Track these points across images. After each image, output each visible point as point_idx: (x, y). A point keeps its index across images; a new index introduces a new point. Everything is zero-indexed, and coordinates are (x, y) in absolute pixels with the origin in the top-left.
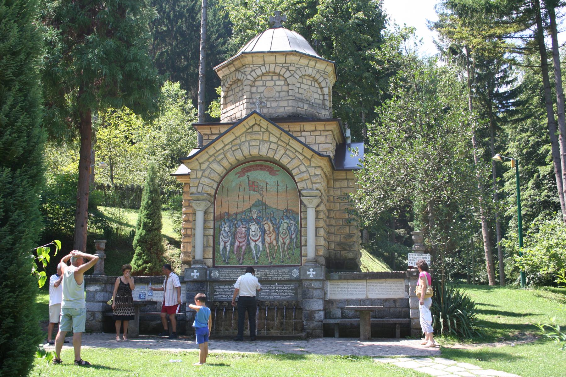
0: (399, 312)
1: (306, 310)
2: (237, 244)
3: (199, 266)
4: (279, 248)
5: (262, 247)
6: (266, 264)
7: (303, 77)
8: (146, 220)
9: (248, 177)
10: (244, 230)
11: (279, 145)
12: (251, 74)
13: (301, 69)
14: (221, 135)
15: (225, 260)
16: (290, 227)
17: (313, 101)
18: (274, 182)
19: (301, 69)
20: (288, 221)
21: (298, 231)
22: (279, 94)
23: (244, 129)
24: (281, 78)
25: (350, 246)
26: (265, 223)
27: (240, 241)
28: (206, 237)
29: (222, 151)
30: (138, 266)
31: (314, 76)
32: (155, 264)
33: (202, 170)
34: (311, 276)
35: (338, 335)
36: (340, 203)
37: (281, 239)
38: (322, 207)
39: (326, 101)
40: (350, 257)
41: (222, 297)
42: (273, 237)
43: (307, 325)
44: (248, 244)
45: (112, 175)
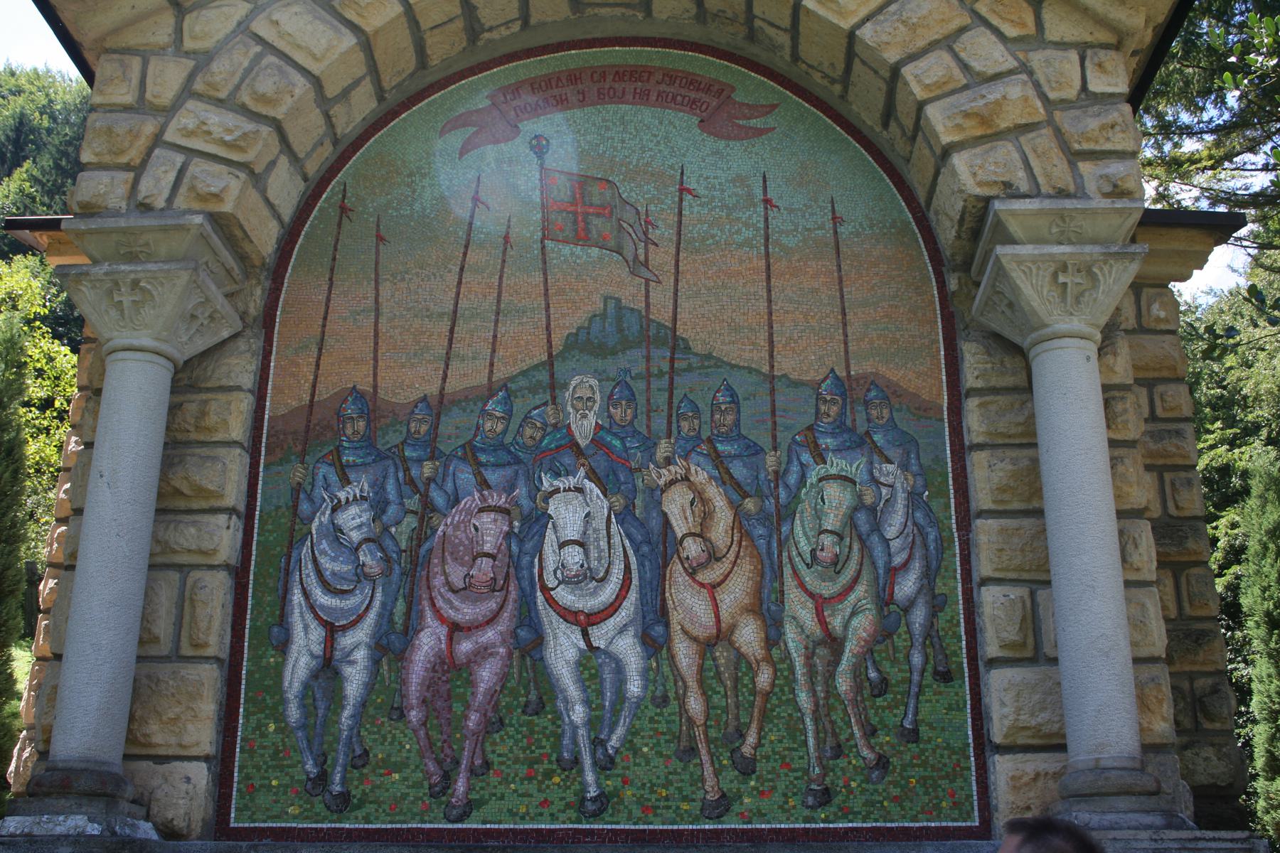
2: (429, 641)
4: (791, 680)
10: (491, 530)
15: (322, 779)
16: (872, 510)
18: (740, 180)
20: (855, 466)
21: (943, 544)
33: (187, 54)
37: (799, 609)
42: (735, 593)
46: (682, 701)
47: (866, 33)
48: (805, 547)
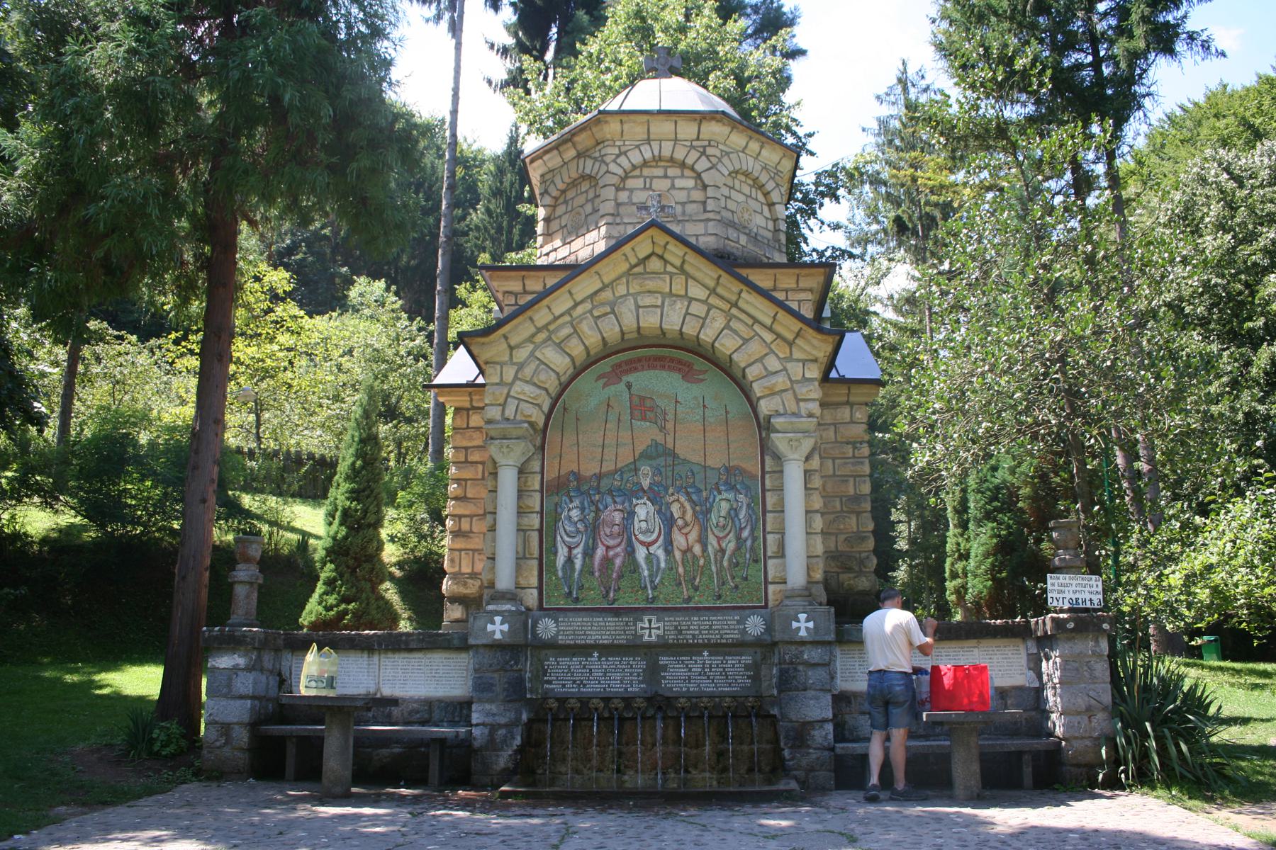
1: (791, 721)
2: (600, 552)
3: (508, 607)
4: (710, 562)
5: (666, 561)
7: (735, 173)
8: (348, 503)
9: (629, 386)
10: (618, 517)
13: (731, 155)
14: (548, 292)
15: (570, 593)
16: (736, 510)
18: (695, 398)
19: (731, 155)
20: (730, 496)
21: (757, 520)
23: (625, 267)
24: (687, 173)
26: (672, 499)
27: (609, 546)
28: (522, 533)
29: (567, 318)
30: (328, 609)
31: (757, 175)
32: (368, 604)
33: (515, 364)
34: (803, 633)
36: (834, 459)
37: (712, 540)
40: (861, 588)
41: (564, 686)
42: (693, 536)
43: (792, 759)
44: (631, 552)
45: (258, 433)
46: (677, 569)
47: (735, 356)
48: (715, 522)
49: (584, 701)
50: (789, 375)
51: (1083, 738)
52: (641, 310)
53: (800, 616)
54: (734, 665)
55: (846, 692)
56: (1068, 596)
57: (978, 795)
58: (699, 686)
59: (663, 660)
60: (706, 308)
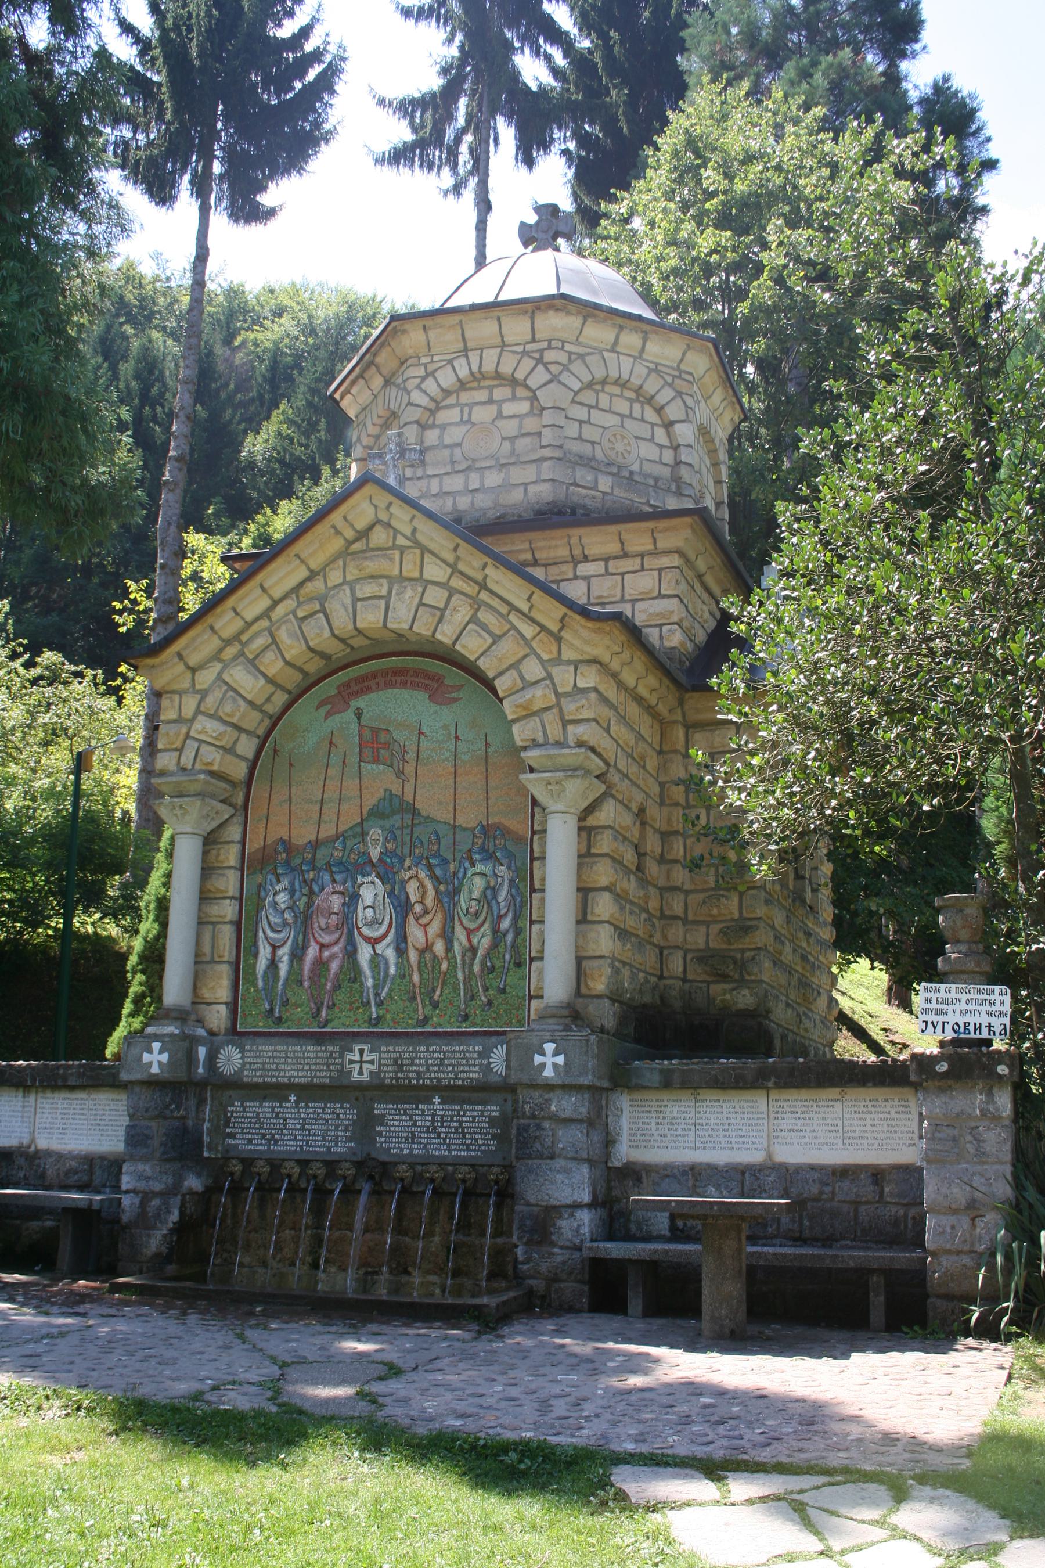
0: (896, 1222)
1: (528, 1204)
2: (312, 952)
3: (172, 1029)
4: (455, 967)
5: (397, 964)
6: (408, 1026)
9: (359, 714)
10: (336, 902)
11: (452, 592)
12: (423, 386)
13: (588, 359)
15: (271, 1011)
16: (494, 888)
17: (635, 467)
18: (445, 727)
19: (588, 359)
21: (523, 903)
22: (513, 443)
23: (338, 544)
24: (521, 392)
25: (742, 966)
26: (408, 874)
29: (265, 623)
31: (638, 382)
33: (197, 692)
34: (548, 1072)
35: (640, 1308)
37: (460, 935)
38: (607, 814)
39: (683, 466)
40: (741, 1006)
41: (250, 1141)
42: (435, 928)
43: (527, 1261)
44: (351, 953)
46: (411, 976)
48: (464, 907)
49: (275, 1164)
50: (554, 684)
51: (959, 1253)
52: (359, 604)
53: (546, 1046)
54: (474, 1117)
55: (634, 1163)
56: (952, 1019)
57: (732, 1332)
58: (425, 1147)
59: (380, 1109)
60: (446, 594)
